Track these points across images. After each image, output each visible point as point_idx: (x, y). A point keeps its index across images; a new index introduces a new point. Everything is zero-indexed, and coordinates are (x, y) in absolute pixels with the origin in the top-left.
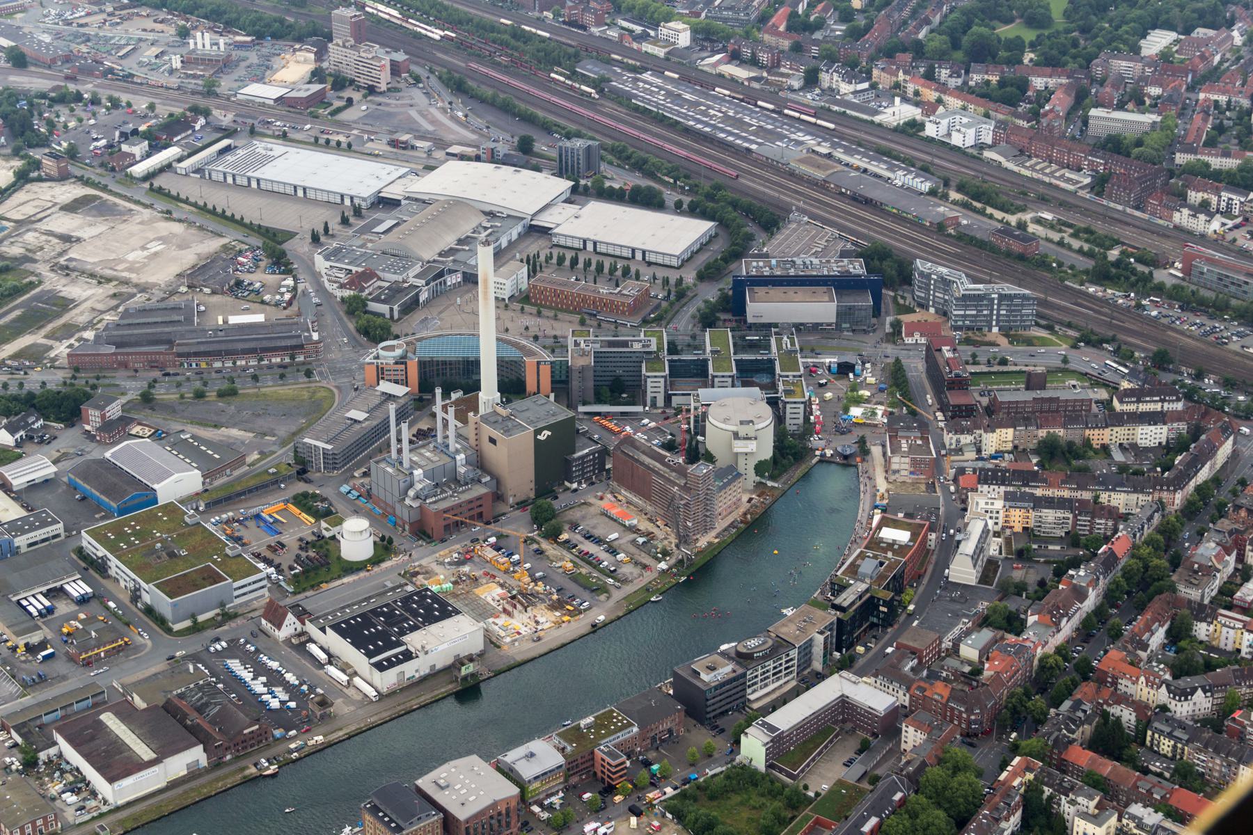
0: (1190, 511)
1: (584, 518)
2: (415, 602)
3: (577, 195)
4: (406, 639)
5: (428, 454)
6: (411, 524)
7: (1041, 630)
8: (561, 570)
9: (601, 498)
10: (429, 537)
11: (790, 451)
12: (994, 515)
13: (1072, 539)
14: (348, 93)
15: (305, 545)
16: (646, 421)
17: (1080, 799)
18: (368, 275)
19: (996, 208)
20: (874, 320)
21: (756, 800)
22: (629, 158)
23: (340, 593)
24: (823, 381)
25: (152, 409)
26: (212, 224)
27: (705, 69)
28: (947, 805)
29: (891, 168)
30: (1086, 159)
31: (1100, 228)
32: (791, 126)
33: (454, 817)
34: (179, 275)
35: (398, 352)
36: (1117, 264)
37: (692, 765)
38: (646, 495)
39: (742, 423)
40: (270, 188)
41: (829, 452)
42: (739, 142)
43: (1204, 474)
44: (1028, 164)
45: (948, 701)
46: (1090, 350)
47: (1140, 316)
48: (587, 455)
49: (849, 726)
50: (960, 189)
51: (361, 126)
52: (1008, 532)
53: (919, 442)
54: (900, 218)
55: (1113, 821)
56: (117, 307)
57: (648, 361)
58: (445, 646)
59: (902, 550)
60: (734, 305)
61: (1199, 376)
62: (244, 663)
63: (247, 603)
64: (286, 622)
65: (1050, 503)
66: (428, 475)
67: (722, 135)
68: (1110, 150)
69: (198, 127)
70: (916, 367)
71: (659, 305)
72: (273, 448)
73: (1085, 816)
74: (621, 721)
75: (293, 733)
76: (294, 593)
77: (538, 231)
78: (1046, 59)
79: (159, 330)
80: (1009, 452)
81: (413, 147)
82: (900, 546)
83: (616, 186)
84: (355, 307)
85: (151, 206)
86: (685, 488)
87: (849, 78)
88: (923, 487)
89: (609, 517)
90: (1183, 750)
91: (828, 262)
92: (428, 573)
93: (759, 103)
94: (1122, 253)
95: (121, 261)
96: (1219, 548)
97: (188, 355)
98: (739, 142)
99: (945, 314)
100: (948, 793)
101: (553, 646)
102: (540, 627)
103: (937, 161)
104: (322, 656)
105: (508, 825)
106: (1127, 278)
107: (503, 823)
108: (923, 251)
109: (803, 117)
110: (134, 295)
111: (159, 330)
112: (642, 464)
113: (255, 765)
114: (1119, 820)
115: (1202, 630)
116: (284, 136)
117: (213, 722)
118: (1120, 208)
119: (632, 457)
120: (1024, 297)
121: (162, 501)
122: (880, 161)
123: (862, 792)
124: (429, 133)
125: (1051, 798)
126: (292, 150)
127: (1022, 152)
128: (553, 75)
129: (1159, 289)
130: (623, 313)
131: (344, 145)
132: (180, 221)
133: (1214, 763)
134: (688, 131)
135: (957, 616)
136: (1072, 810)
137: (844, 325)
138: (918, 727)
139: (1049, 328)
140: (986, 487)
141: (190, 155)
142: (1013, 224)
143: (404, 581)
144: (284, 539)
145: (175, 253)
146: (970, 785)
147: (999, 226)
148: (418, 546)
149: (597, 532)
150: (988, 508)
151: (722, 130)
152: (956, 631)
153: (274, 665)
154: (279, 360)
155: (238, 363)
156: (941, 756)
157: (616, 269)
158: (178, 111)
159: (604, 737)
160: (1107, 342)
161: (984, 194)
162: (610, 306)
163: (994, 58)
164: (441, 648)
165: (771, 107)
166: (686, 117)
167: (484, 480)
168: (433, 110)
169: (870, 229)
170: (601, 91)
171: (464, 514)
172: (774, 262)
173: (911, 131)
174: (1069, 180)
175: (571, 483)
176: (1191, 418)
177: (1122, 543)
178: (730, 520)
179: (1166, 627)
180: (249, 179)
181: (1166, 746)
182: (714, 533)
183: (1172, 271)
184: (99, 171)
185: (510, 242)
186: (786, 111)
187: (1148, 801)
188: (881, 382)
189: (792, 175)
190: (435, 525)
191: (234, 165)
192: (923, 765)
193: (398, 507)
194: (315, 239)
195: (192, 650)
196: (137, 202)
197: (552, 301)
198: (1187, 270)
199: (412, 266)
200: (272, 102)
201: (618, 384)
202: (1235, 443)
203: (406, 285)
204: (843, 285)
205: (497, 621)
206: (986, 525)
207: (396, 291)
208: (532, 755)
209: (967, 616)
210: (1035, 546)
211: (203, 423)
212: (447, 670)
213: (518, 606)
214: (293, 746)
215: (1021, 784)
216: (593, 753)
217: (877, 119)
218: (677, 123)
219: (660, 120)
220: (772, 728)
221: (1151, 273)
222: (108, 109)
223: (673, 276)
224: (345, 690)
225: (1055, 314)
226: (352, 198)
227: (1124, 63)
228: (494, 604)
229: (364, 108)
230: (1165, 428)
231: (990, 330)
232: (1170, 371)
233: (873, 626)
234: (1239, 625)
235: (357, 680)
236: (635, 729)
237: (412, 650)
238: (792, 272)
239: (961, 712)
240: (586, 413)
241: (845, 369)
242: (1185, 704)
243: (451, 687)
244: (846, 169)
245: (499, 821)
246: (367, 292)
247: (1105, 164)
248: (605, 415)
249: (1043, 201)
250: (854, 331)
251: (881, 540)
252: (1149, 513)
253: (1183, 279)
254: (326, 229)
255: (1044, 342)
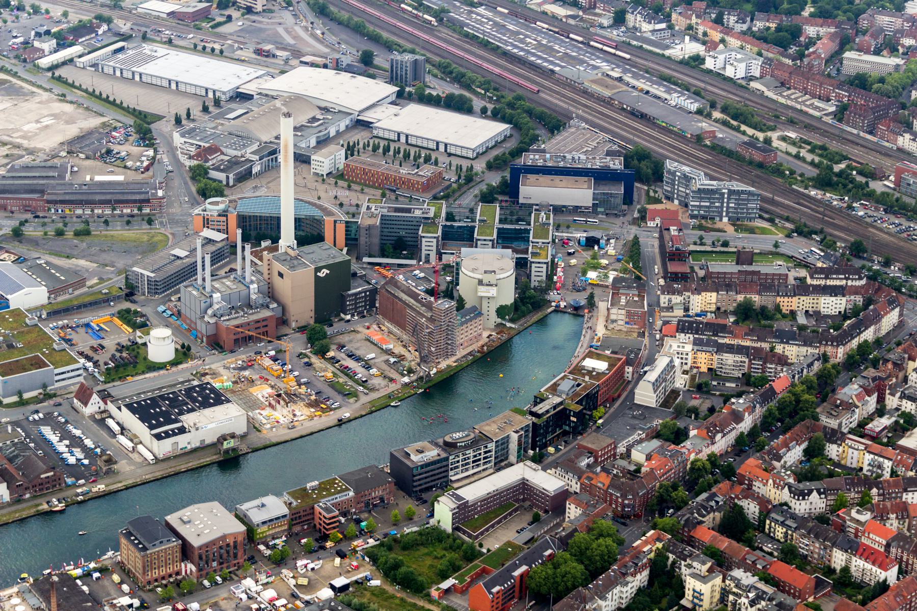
0: (852, 364)
1: (351, 341)
2: (196, 392)
3: (402, 97)
4: (182, 418)
5: (228, 283)
6: (208, 337)
7: (698, 441)
8: (323, 379)
9: (368, 328)
10: (221, 347)
11: (529, 303)
12: (684, 356)
13: (747, 380)
14: (230, 11)
15: (121, 348)
16: (417, 272)
17: (695, 564)
18: (213, 150)
19: (750, 127)
20: (625, 207)
21: (440, 552)
22: (451, 73)
23: (141, 385)
24: (572, 251)
25: (20, 242)
26: (97, 106)
27: (533, 7)
28: (587, 562)
29: (668, 91)
30: (834, 92)
31: (834, 146)
32: (592, 54)
33: (190, 544)
34: (62, 143)
35: (221, 207)
36: (841, 174)
37: (395, 525)
38: (401, 325)
39: (486, 272)
40: (149, 81)
41: (563, 304)
42: (545, 64)
43: (868, 335)
44: (785, 94)
45: (608, 488)
46: (801, 240)
47: (849, 215)
48: (360, 293)
49: (527, 503)
50: (724, 110)
51: (235, 38)
52: (695, 371)
53: (636, 299)
54: (667, 131)
55: (718, 581)
56: (7, 164)
57: (425, 224)
58: (213, 425)
59: (600, 375)
60: (510, 189)
61: (887, 264)
62: (54, 430)
63: (65, 387)
64: (92, 401)
65: (730, 349)
66: (226, 298)
67: (533, 59)
68: (857, 86)
69: (100, 32)
70: (650, 244)
71: (450, 185)
72: (110, 276)
73: (695, 576)
74: (339, 486)
75: (82, 482)
76: (105, 382)
77: (363, 125)
78: (821, 12)
79: (35, 182)
80: (711, 312)
81: (274, 56)
82: (598, 373)
83: (435, 93)
84: (198, 173)
85: (50, 90)
86: (431, 320)
87: (649, 19)
88: (635, 335)
89: (372, 342)
90: (792, 536)
91: (594, 158)
92: (215, 374)
93: (571, 36)
94: (848, 166)
95: (17, 130)
96: (861, 389)
97: (55, 202)
98: (545, 64)
99: (686, 206)
100: (589, 553)
101: (304, 433)
102: (295, 419)
103: (710, 88)
104: (116, 428)
105: (235, 556)
106: (845, 186)
107: (231, 553)
108: (676, 154)
109: (605, 48)
110: (23, 156)
111: (35, 182)
112: (400, 300)
113: (48, 503)
114: (724, 581)
115: (833, 450)
116: (170, 42)
117: (18, 469)
118: (855, 131)
119: (394, 295)
120: (750, 193)
121: (13, 306)
122: (660, 85)
123: (523, 549)
124: (290, 45)
125: (674, 563)
126: (173, 53)
127: (783, 84)
128: (402, 6)
129: (870, 195)
130: (418, 190)
131: (217, 52)
132: (71, 102)
133: (814, 546)
134: (506, 55)
135: (634, 428)
136: (689, 571)
137: (599, 210)
138: (578, 505)
139: (771, 221)
140: (683, 335)
141: (89, 53)
142: (761, 139)
143: (193, 377)
144: (104, 343)
145: (62, 126)
146: (607, 547)
147: (746, 139)
148: (211, 355)
149: (358, 353)
150: (680, 348)
151: (534, 55)
152: (631, 439)
153: (78, 433)
154: (129, 211)
155: (96, 211)
156: (591, 526)
157: (420, 156)
158: (85, 18)
159: (325, 496)
160: (816, 233)
161: (741, 114)
162: (407, 184)
163: (776, 8)
164: (210, 426)
165: (580, 39)
166: (506, 43)
167: (271, 306)
168: (297, 28)
169: (634, 135)
170: (440, 21)
171: (252, 332)
172: (548, 156)
173: (693, 64)
174: (817, 108)
175: (346, 314)
176: (867, 291)
177: (781, 381)
178: (470, 349)
179: (804, 445)
180: (133, 73)
181: (780, 532)
182: (454, 358)
183: (886, 183)
184: (13, 61)
185: (338, 132)
186: (592, 43)
187: (751, 568)
188: (620, 254)
189: (585, 93)
190: (227, 339)
191: (123, 62)
192: (575, 530)
193: (199, 322)
194: (178, 121)
195: (14, 419)
196: (40, 87)
197: (361, 179)
198: (898, 183)
199: (250, 145)
200: (165, 16)
201: (399, 243)
202: (901, 315)
203: (243, 159)
204: (601, 176)
205: (262, 412)
206: (672, 361)
207: (234, 163)
208: (263, 505)
209: (641, 429)
210: (715, 383)
211: (58, 254)
212: (213, 445)
213: (282, 402)
214: (79, 490)
215: (651, 551)
216: (313, 508)
217: (667, 53)
218: (498, 47)
219: (485, 45)
220: (459, 498)
221: (867, 183)
222: (29, 14)
223: (465, 164)
224: (130, 454)
225: (778, 210)
226: (214, 92)
227: (887, 19)
228: (263, 400)
229: (240, 23)
230: (844, 299)
231: (721, 220)
232: (864, 259)
233: (565, 433)
234: (862, 447)
235: (140, 448)
236: (351, 494)
237: (186, 426)
238: (561, 164)
239: (617, 497)
240: (369, 263)
241: (591, 242)
242: (803, 502)
243: (215, 458)
244: (630, 90)
245: (228, 552)
246: (210, 163)
247: (849, 96)
248: (385, 266)
249: (792, 122)
250: (607, 214)
251: (583, 368)
252: (810, 361)
253: (894, 189)
254: (188, 115)
255: (763, 231)
